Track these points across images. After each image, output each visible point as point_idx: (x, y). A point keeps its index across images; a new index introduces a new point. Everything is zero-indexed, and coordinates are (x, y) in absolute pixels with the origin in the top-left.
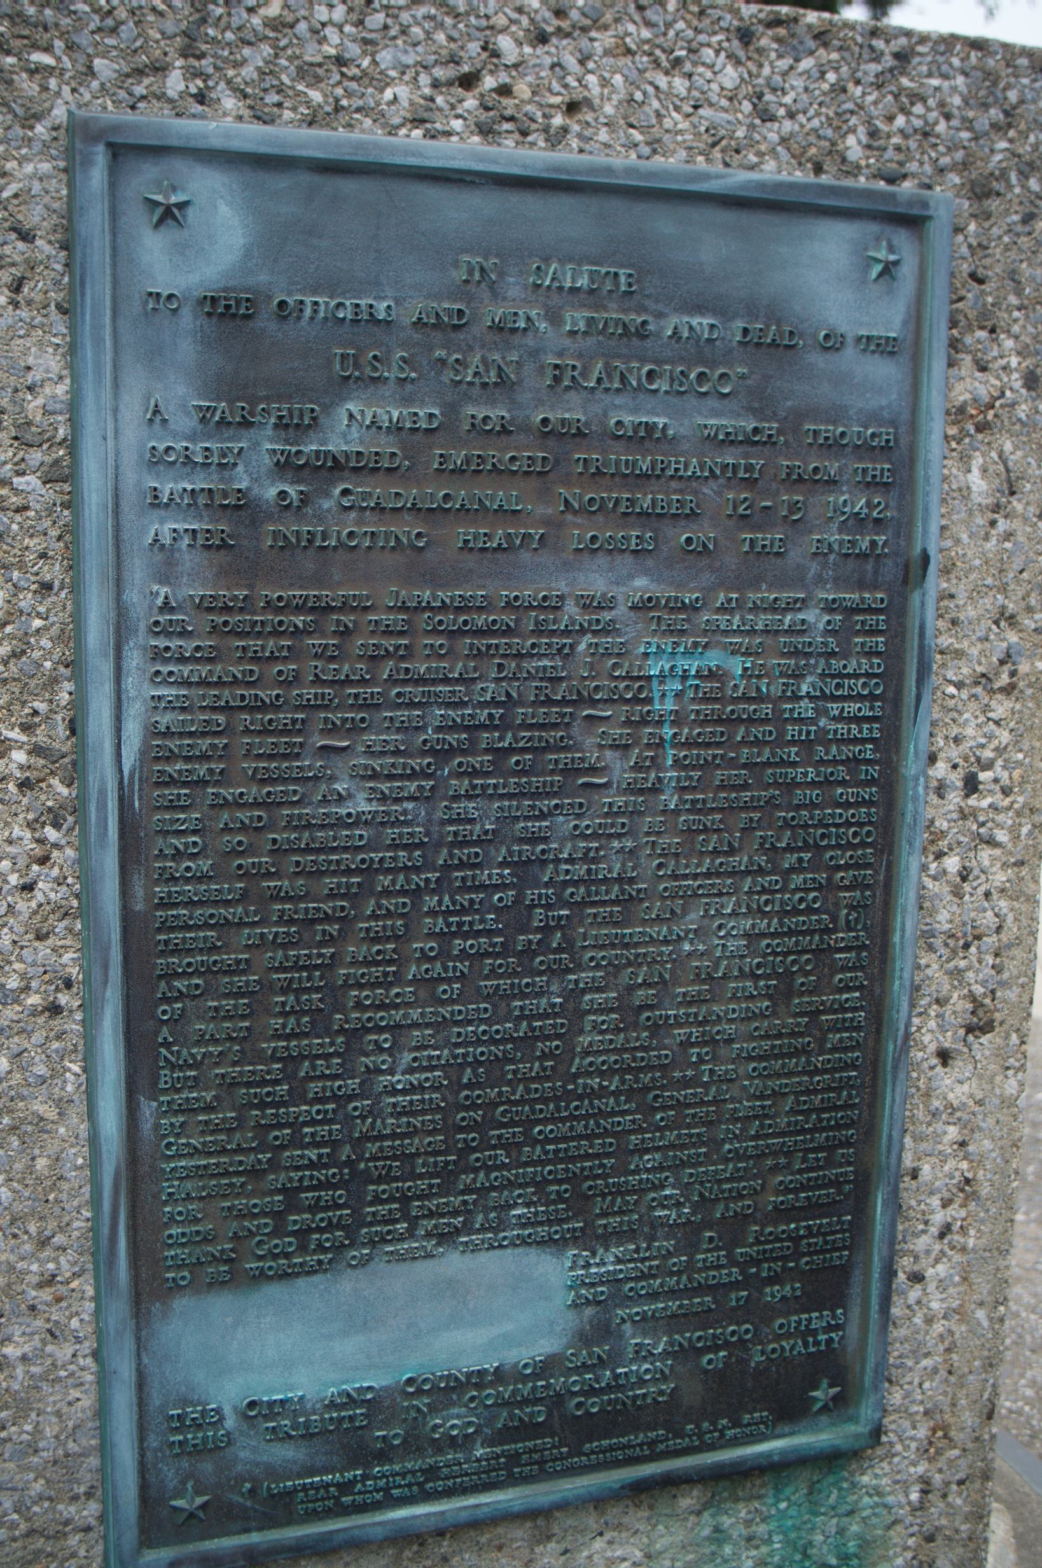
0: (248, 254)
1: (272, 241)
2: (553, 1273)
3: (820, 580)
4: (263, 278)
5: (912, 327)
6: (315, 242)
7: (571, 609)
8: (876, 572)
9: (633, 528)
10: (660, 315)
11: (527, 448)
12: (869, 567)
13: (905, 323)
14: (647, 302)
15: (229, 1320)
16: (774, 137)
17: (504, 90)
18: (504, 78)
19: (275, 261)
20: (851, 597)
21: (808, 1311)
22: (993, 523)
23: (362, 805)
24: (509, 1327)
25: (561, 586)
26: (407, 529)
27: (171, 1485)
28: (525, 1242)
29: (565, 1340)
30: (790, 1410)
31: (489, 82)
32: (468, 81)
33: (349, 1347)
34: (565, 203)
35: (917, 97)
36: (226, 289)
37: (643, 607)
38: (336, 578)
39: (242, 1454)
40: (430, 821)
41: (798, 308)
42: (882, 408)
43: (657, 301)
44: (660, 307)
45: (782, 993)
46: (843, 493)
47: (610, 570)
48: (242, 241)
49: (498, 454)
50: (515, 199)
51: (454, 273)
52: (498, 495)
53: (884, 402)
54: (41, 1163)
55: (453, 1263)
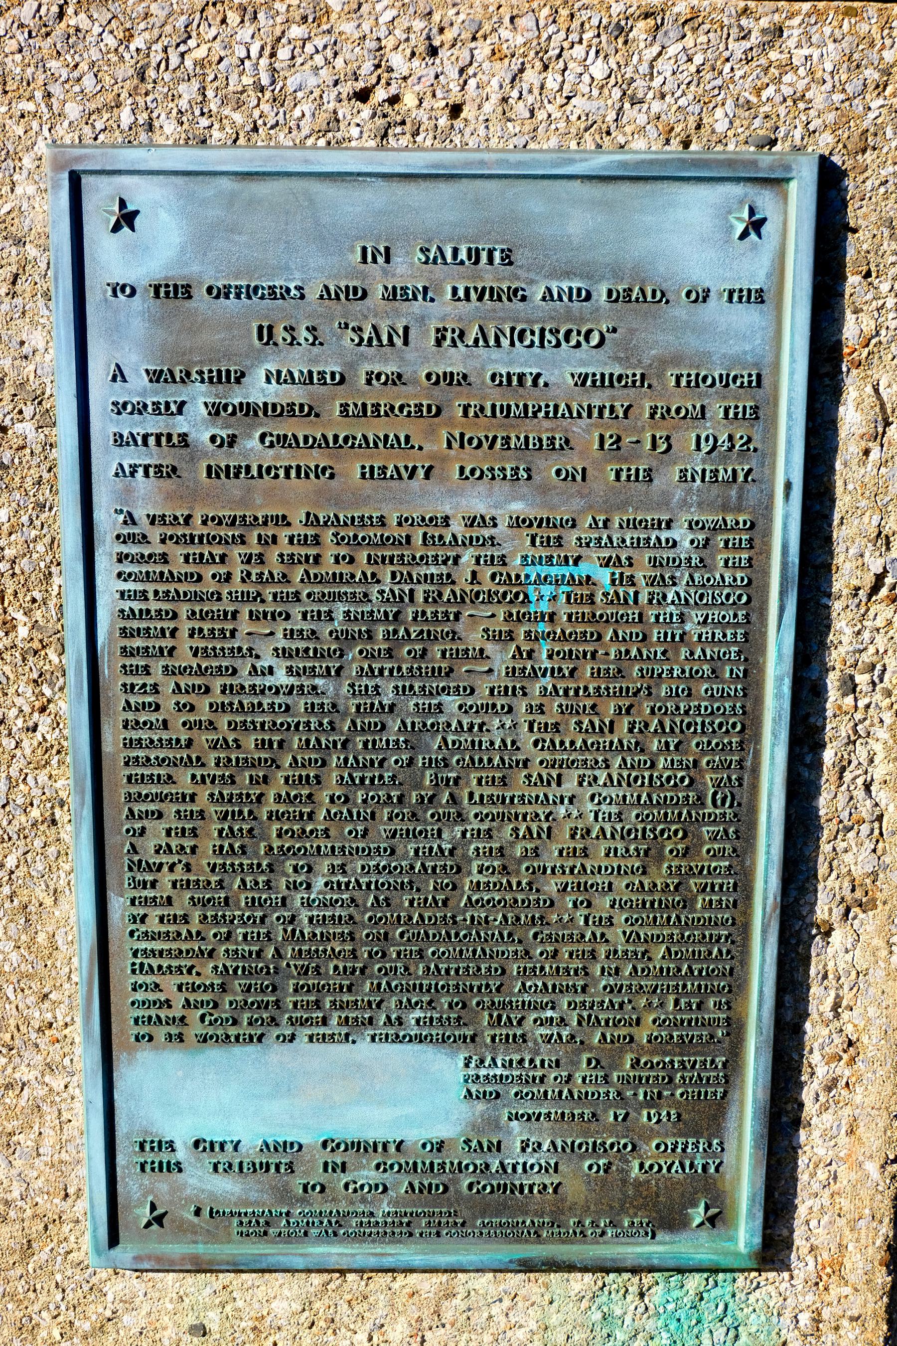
0: (183, 250)
1: (202, 238)
2: (447, 1068)
3: (684, 504)
4: (195, 268)
5: (775, 279)
6: (237, 238)
7: (457, 527)
8: (740, 498)
9: (509, 460)
10: (532, 282)
11: (415, 396)
12: (733, 493)
13: (769, 276)
14: (519, 272)
15: (180, 1073)
16: (642, 119)
17: (394, 100)
18: (393, 90)
19: (205, 254)
20: (709, 518)
21: (686, 1136)
22: (867, 452)
23: (282, 678)
24: (409, 1110)
25: (446, 509)
26: (315, 458)
27: (136, 1197)
28: (420, 1039)
29: (459, 1129)
30: (670, 1220)
31: (380, 94)
32: (363, 96)
33: (276, 1107)
34: (444, 189)
35: (789, 66)
36: (166, 278)
37: (518, 523)
38: (258, 502)
39: (191, 1181)
40: (337, 695)
41: (662, 269)
42: (745, 353)
43: (529, 270)
44: (532, 275)
45: (651, 855)
46: (706, 428)
47: (489, 496)
48: (178, 240)
49: (397, 397)
50: (401, 190)
51: (350, 257)
52: (400, 428)
53: (748, 347)
54: (41, 938)
55: (364, 1049)
